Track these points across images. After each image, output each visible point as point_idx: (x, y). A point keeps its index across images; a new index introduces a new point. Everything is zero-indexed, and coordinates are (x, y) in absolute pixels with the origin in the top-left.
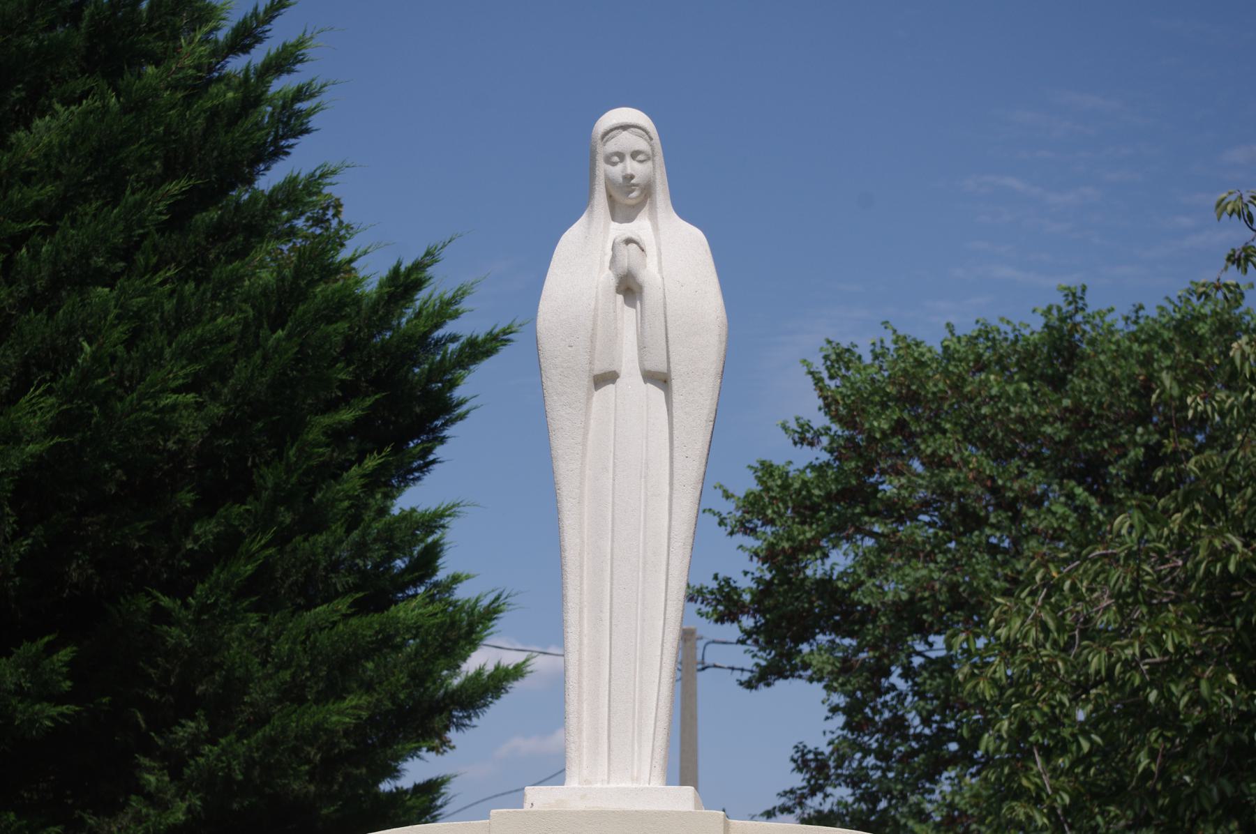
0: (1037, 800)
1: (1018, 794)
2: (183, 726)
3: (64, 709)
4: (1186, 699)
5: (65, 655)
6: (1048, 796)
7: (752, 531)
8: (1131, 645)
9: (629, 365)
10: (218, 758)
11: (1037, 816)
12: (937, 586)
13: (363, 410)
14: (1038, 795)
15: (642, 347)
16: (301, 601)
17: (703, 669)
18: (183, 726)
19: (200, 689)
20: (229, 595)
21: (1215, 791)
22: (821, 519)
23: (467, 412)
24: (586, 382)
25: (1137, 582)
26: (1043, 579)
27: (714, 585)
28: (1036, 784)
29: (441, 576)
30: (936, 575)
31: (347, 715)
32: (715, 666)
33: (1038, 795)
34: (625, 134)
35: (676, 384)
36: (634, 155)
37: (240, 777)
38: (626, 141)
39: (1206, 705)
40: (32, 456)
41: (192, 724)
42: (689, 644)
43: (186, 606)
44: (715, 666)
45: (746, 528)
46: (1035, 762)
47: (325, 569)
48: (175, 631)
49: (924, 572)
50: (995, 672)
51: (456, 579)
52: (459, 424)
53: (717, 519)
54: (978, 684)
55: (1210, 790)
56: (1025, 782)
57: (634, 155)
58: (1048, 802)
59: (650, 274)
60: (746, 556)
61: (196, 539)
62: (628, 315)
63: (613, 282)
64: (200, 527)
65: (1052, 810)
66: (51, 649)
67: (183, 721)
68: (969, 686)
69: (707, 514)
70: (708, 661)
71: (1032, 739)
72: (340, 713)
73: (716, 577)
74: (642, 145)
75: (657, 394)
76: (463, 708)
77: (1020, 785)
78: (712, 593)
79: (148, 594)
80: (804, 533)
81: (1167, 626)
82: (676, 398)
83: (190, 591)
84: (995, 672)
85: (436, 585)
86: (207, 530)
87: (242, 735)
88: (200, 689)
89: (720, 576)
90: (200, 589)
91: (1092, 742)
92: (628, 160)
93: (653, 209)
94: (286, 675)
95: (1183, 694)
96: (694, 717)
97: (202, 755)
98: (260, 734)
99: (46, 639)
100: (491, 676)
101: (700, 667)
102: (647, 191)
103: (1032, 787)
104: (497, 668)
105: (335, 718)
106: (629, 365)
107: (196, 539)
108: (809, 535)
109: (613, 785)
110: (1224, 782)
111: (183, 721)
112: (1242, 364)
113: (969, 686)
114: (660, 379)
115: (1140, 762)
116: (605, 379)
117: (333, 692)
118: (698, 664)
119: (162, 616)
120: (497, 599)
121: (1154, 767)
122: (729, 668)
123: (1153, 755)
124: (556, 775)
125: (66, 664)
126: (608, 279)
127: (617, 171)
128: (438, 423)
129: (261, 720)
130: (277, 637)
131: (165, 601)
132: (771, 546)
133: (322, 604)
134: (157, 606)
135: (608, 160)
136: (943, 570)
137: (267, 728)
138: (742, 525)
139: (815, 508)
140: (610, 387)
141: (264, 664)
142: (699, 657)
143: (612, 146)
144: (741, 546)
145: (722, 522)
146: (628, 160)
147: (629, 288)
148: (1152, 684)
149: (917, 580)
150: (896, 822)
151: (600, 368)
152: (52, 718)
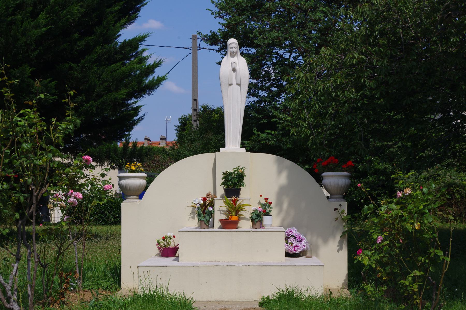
0: (305, 121)
1: (300, 118)
2: (78, 98)
3: (54, 97)
4: (341, 95)
5: (54, 83)
6: (307, 119)
7: (222, 17)
8: (329, 83)
9: (234, 83)
10: (89, 107)
11: (304, 124)
12: (281, 38)
13: (120, 6)
14: (305, 119)
15: (236, 80)
16: (107, 63)
17: (200, 49)
18: (78, 98)
19: (81, 87)
20: (91, 64)
21: (347, 118)
22: (245, 14)
23: (147, 3)
24: (228, 85)
25: (332, 65)
26: (309, 61)
27: (210, 34)
28: (304, 116)
29: (140, 49)
30: (280, 35)
31: (123, 95)
32: (204, 48)
33: (305, 119)
34: (233, 44)
35: (242, 86)
36: (234, 47)
37: (95, 112)
38: (233, 45)
39: (345, 97)
40: (44, 31)
41: (81, 98)
42: (194, 40)
43: (78, 66)
44: (204, 48)
45: (221, 16)
46: (305, 111)
47: (113, 54)
48: (75, 73)
49: (277, 34)
50: (295, 87)
51: (143, 50)
52: (145, 6)
53: (211, 12)
54: (291, 90)
55: (346, 118)
56: (302, 116)
57: (234, 47)
58: (307, 121)
59: (237, 68)
60: (221, 26)
61: (79, 47)
62: (234, 74)
63: (232, 69)
64: (80, 43)
65: (308, 122)
66: (51, 81)
67: (78, 97)
68: (289, 90)
69: (208, 10)
70: (201, 47)
71: (304, 105)
72: (121, 94)
73: (211, 32)
74: (236, 46)
75: (239, 87)
76: (150, 89)
77: (301, 116)
78: (209, 36)
79: (68, 63)
80: (240, 19)
81: (338, 77)
82: (242, 88)
83: (80, 62)
84: (295, 87)
85: (138, 52)
86: (81, 44)
87: (96, 101)
88: (81, 87)
89: (212, 32)
90: (82, 62)
91: (319, 105)
92: (234, 48)
93: (237, 55)
94: (106, 84)
95: (341, 94)
96: (196, 66)
97: (84, 106)
98: (100, 101)
99: (49, 79)
100: (157, 80)
101: (198, 49)
102: (236, 53)
103: (303, 117)
104: (158, 77)
105: (120, 96)
106: (234, 83)
107: (79, 47)
108: (241, 20)
109: (233, 148)
110: (349, 116)
111: (78, 97)
112: (360, 9)
113: (289, 90)
114: (239, 85)
115: (329, 111)
116: (231, 85)
117: (117, 89)
118: (198, 48)
119: (71, 68)
120: (160, 61)
121: (333, 112)
122: (208, 49)
123: (333, 109)
124: (224, 146)
125: (55, 85)
126: (231, 68)
127: (232, 50)
128: (138, 6)
129: (99, 96)
130: (102, 74)
131: (73, 65)
132: (229, 24)
133: (113, 64)
134: (70, 66)
135: (230, 48)
136: (283, 33)
137: (102, 99)
138: (219, 14)
139: (243, 10)
140: (231, 86)
141: (99, 81)
142: (198, 45)
143: (231, 46)
144: (219, 23)
145: (212, 14)
146: (234, 48)
147: (234, 70)
148: (334, 92)
149: (274, 37)
150: (268, 110)
151: (230, 83)
152: (51, 100)
